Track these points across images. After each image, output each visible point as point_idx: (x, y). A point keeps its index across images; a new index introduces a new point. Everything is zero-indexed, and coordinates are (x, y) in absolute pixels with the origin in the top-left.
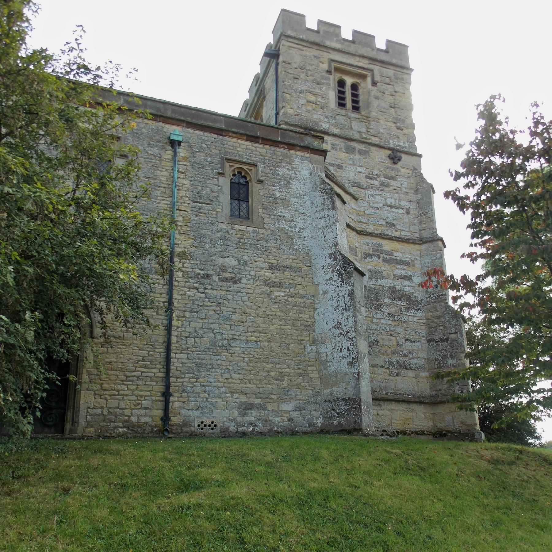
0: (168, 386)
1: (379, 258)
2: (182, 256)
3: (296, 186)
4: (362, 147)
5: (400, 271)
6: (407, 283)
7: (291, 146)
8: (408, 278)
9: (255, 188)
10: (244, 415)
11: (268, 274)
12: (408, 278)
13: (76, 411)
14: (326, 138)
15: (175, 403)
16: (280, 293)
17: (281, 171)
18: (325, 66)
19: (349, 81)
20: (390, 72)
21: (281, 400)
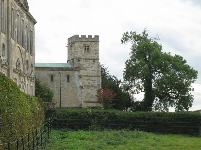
2: (62, 88)
3: (75, 76)
4: (88, 60)
5: (93, 82)
6: (94, 84)
7: (75, 70)
8: (95, 83)
11: (72, 89)
12: (95, 83)
14: (82, 77)
15: (61, 105)
16: (73, 91)
19: (87, 46)
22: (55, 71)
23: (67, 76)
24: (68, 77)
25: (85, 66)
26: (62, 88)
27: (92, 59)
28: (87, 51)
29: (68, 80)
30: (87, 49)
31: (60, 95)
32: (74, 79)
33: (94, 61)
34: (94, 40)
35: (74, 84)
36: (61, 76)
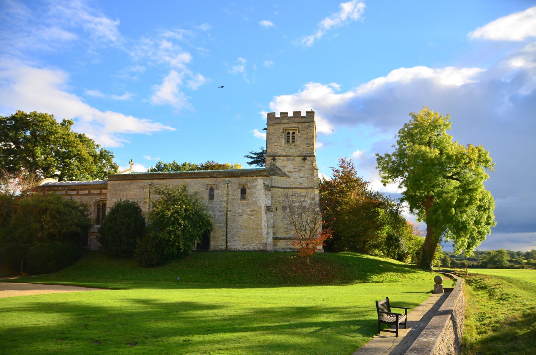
0: (227, 241)
1: (296, 196)
2: (230, 211)
3: (258, 187)
4: (293, 158)
9: (247, 190)
10: (243, 246)
11: (250, 213)
13: (210, 246)
15: (229, 244)
16: (253, 217)
17: (254, 184)
18: (282, 131)
19: (291, 132)
20: (306, 125)
21: (252, 243)
22: (218, 179)
23: (241, 187)
24: (243, 191)
25: (286, 170)
26: (230, 211)
27: (299, 156)
28: (291, 141)
29: (243, 198)
30: (291, 138)
31: (227, 225)
32: (255, 193)
33: (304, 159)
34: (304, 120)
35: (255, 203)
36: (229, 188)
